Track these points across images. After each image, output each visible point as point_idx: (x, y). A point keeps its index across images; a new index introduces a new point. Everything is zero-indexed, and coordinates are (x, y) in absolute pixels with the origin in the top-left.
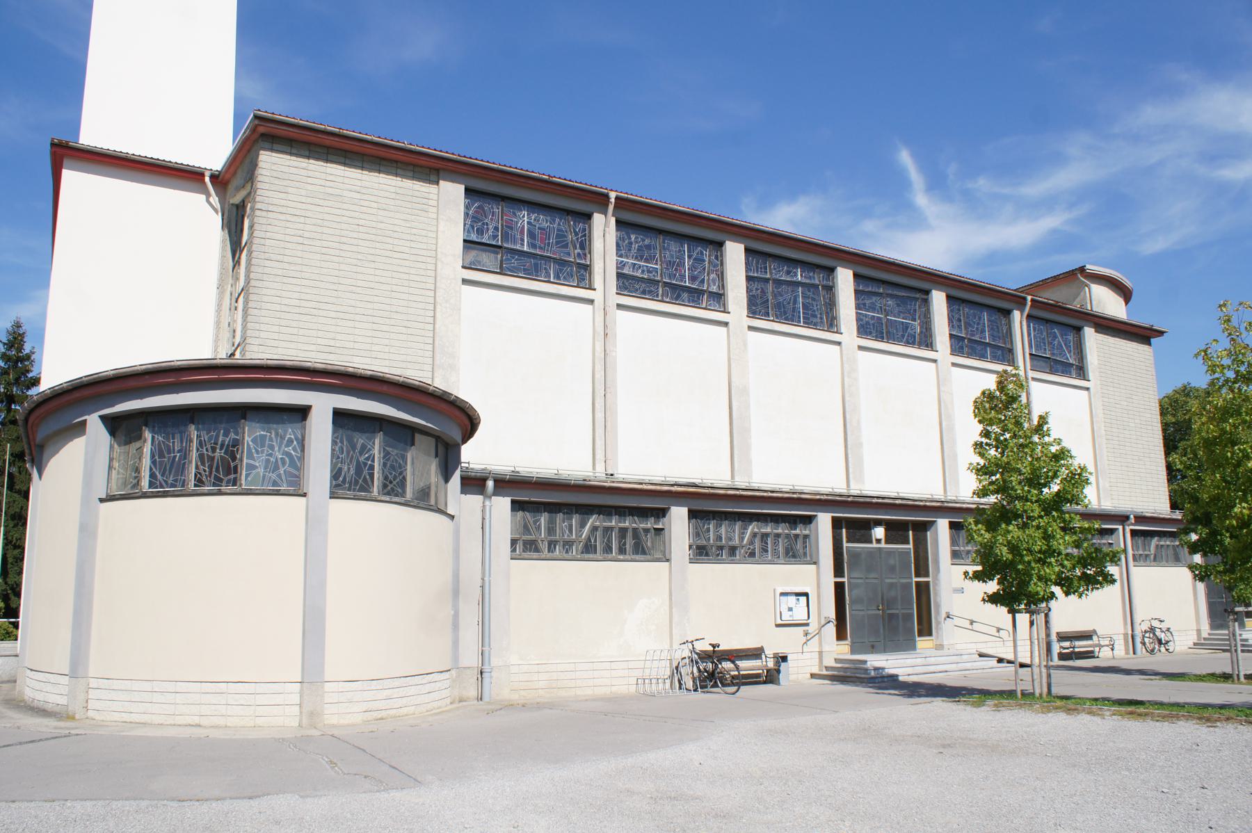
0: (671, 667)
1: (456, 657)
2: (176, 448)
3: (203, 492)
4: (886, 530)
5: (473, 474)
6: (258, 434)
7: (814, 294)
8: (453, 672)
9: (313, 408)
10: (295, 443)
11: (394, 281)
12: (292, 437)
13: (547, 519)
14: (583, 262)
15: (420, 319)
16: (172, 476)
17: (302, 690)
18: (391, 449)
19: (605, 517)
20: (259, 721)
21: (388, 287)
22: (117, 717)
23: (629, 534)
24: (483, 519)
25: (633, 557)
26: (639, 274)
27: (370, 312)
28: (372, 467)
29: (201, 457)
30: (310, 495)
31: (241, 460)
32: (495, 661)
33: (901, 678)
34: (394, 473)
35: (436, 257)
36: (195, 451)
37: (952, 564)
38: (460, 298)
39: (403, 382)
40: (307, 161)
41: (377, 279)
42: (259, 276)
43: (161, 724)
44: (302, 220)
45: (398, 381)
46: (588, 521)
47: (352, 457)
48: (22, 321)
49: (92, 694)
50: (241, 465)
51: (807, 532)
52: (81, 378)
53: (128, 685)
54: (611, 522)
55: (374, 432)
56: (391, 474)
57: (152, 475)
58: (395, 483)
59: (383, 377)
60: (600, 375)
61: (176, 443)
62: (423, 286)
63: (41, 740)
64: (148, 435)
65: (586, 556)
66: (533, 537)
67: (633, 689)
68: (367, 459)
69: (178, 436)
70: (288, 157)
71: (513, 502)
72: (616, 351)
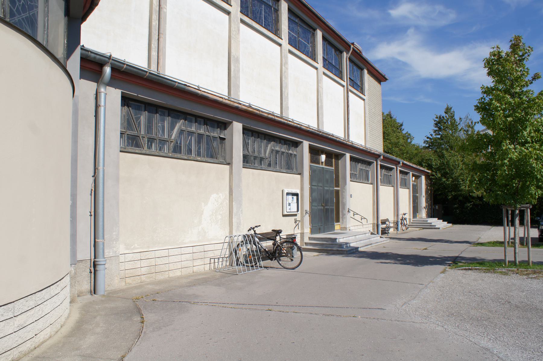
0: (230, 249)
4: (326, 157)
5: (93, 55)
7: (269, 11)
32: (108, 253)
33: (360, 249)
37: (351, 181)
51: (295, 153)
60: (155, 23)
66: (135, 133)
72: (166, 9)
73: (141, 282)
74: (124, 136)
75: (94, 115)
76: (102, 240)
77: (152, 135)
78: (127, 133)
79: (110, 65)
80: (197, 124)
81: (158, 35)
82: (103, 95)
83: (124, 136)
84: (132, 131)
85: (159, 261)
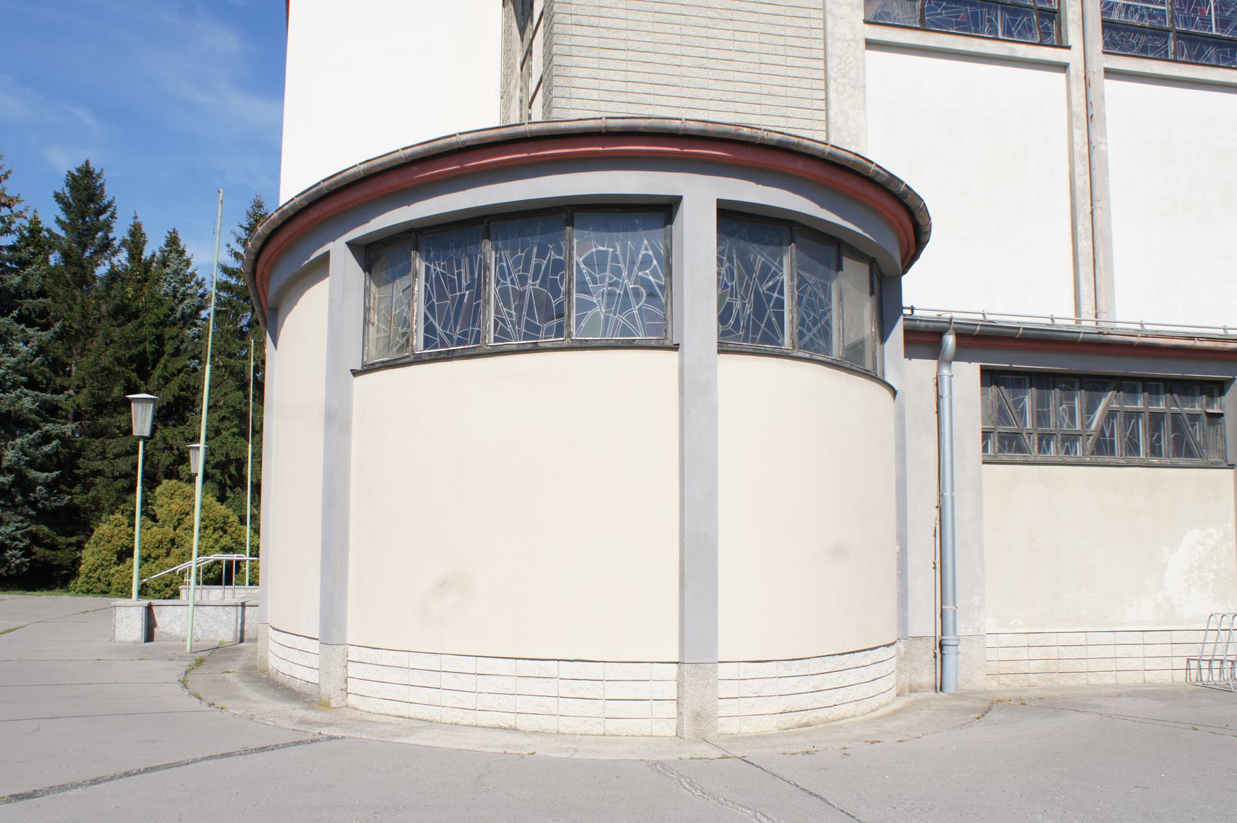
1: (903, 622)
2: (463, 282)
3: (508, 348)
5: (923, 324)
6: (594, 250)
8: (901, 645)
9: (684, 200)
10: (655, 262)
11: (764, 48)
12: (650, 253)
13: (1035, 400)
14: (1047, 6)
15: (805, 104)
16: (458, 328)
17: (680, 674)
18: (807, 275)
19: (1125, 394)
20: (612, 726)
21: (755, 58)
22: (389, 707)
23: (1167, 423)
24: (939, 397)
25: (1175, 460)
26: (1135, 20)
27: (730, 96)
28: (780, 304)
29: (504, 293)
30: (686, 347)
31: (569, 293)
32: (963, 628)
34: (813, 314)
35: (824, 7)
36: (493, 285)
38: (864, 67)
39: (830, 154)
41: (738, 46)
42: (566, 50)
43: (456, 724)
45: (823, 152)
46: (1100, 401)
47: (748, 284)
48: (262, 199)
49: (353, 670)
50: (569, 303)
52: (318, 184)
53: (402, 659)
54: (1136, 404)
55: (780, 244)
56: (809, 315)
57: (429, 329)
58: (814, 330)
59: (799, 145)
60: (1082, 181)
61: (463, 275)
62: (808, 53)
63: (277, 747)
64: (420, 264)
65: (1100, 459)
66: (1014, 428)
67: (1180, 676)
68: (772, 289)
69: (465, 261)
71: (985, 372)
72: (1106, 144)
73: (1029, 686)
74: (994, 437)
75: (936, 410)
76: (951, 607)
77: (1050, 427)
78: (998, 430)
79: (953, 332)
80: (1146, 394)
81: (1092, 205)
82: (946, 380)
83: (994, 437)
84: (1010, 425)
85: (1066, 652)
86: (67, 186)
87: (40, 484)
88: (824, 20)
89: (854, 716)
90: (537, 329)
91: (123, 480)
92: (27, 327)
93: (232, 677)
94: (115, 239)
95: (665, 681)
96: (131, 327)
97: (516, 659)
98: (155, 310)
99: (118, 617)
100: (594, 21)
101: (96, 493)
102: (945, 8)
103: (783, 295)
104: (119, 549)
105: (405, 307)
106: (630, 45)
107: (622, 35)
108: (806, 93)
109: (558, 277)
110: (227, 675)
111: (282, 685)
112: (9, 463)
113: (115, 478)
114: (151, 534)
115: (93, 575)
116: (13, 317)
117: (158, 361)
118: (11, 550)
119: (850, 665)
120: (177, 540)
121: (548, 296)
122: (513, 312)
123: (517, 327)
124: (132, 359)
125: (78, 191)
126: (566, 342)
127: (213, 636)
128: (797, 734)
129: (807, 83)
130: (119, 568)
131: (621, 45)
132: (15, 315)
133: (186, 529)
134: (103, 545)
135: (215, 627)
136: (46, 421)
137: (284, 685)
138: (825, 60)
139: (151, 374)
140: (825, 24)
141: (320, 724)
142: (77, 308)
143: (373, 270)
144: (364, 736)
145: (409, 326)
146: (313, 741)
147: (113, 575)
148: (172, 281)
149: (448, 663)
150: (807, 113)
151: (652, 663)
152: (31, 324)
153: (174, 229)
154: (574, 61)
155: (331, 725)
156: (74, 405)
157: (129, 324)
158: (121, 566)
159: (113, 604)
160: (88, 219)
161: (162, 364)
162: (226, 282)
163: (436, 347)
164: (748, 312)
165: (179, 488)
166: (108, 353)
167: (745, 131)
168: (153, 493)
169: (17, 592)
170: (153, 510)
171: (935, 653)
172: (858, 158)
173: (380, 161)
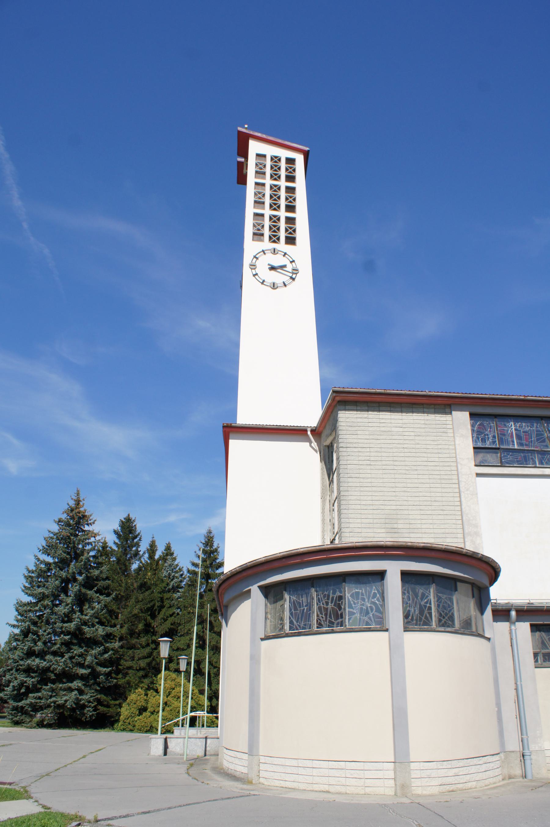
1: (502, 743)
2: (304, 603)
5: (500, 607)
6: (354, 591)
8: (502, 755)
10: (378, 595)
11: (431, 481)
16: (303, 622)
18: (441, 595)
20: (368, 790)
21: (428, 485)
22: (277, 783)
27: (417, 503)
28: (430, 608)
29: (320, 608)
30: (391, 630)
31: (345, 609)
32: (533, 747)
39: (445, 549)
40: (367, 413)
41: (420, 481)
42: (346, 489)
43: (305, 790)
44: (368, 450)
45: (442, 548)
48: (212, 529)
49: (262, 767)
50: (345, 613)
53: (282, 761)
55: (429, 584)
56: (443, 612)
57: (291, 622)
59: (431, 547)
62: (451, 481)
64: (287, 596)
68: (426, 603)
70: (355, 412)
71: (531, 625)
78: (542, 652)
79: (514, 610)
86: (119, 526)
87: (102, 674)
88: (457, 466)
89: (476, 788)
90: (333, 623)
91: (142, 671)
92: (100, 595)
93: (208, 772)
94: (140, 551)
95: (389, 771)
96: (148, 594)
97: (328, 761)
98: (160, 585)
99: (152, 743)
100: (357, 475)
101: (129, 678)
102: (511, 455)
103: (431, 605)
104: (140, 707)
105: (281, 613)
106: (373, 484)
107: (369, 480)
108: (451, 499)
109: (341, 602)
110: (205, 770)
111: (230, 775)
112: (88, 663)
113: (138, 670)
114: (156, 700)
115: (127, 721)
116: (94, 591)
117: (161, 611)
118: (88, 708)
119: (471, 764)
120: (168, 703)
121: (337, 610)
122: (324, 616)
123: (325, 622)
124: (148, 609)
125: (125, 529)
126: (344, 629)
127: (194, 753)
128: (446, 795)
129: (452, 495)
130: (139, 717)
131: (369, 485)
132: (95, 590)
133: (173, 697)
134: (132, 705)
135: (195, 749)
136: (107, 642)
137: (231, 775)
138: (459, 483)
139: (157, 617)
140: (457, 468)
141: (249, 790)
142: (123, 585)
143: (268, 597)
144: (267, 794)
145: (283, 621)
146: (247, 796)
147: (136, 721)
148: (168, 570)
149: (301, 763)
150: (452, 508)
151: (383, 762)
152: (101, 594)
153: (169, 542)
154: (350, 493)
155: (254, 790)
156: (120, 633)
157: (147, 592)
158: (140, 717)
159: (150, 737)
160: (129, 542)
161: (163, 612)
162: (194, 571)
163: (294, 630)
164: (417, 613)
165: (169, 675)
166: (137, 607)
167: (409, 544)
168: (157, 677)
169: (89, 730)
170: (156, 687)
171: (521, 759)
172: (457, 548)
173: (270, 557)
